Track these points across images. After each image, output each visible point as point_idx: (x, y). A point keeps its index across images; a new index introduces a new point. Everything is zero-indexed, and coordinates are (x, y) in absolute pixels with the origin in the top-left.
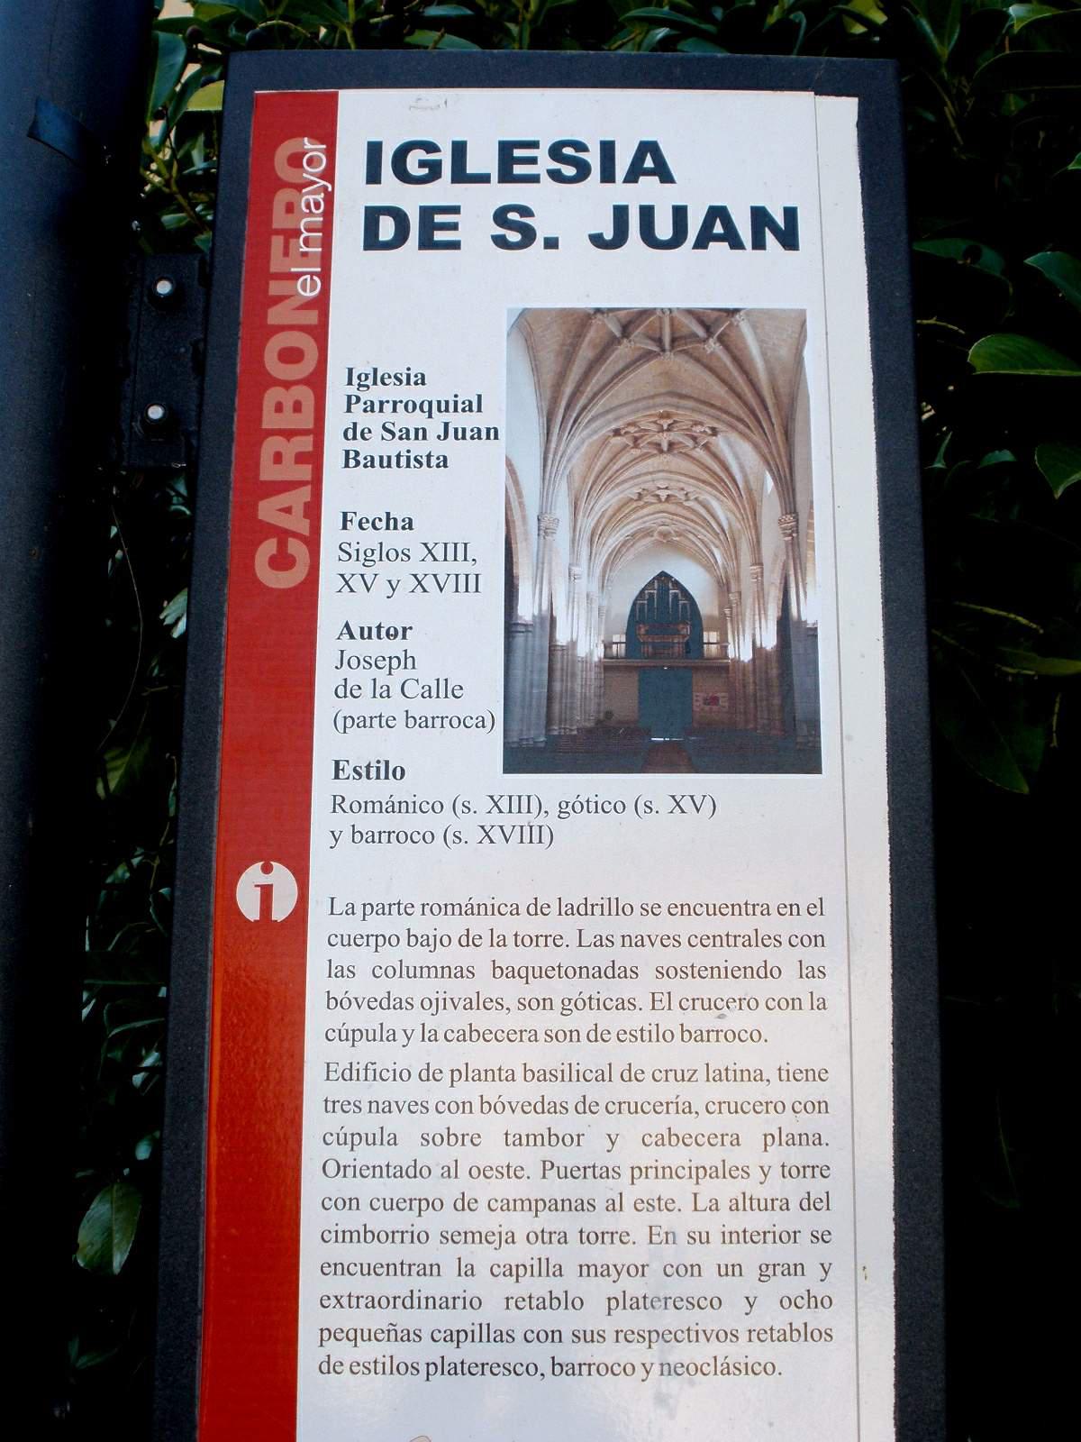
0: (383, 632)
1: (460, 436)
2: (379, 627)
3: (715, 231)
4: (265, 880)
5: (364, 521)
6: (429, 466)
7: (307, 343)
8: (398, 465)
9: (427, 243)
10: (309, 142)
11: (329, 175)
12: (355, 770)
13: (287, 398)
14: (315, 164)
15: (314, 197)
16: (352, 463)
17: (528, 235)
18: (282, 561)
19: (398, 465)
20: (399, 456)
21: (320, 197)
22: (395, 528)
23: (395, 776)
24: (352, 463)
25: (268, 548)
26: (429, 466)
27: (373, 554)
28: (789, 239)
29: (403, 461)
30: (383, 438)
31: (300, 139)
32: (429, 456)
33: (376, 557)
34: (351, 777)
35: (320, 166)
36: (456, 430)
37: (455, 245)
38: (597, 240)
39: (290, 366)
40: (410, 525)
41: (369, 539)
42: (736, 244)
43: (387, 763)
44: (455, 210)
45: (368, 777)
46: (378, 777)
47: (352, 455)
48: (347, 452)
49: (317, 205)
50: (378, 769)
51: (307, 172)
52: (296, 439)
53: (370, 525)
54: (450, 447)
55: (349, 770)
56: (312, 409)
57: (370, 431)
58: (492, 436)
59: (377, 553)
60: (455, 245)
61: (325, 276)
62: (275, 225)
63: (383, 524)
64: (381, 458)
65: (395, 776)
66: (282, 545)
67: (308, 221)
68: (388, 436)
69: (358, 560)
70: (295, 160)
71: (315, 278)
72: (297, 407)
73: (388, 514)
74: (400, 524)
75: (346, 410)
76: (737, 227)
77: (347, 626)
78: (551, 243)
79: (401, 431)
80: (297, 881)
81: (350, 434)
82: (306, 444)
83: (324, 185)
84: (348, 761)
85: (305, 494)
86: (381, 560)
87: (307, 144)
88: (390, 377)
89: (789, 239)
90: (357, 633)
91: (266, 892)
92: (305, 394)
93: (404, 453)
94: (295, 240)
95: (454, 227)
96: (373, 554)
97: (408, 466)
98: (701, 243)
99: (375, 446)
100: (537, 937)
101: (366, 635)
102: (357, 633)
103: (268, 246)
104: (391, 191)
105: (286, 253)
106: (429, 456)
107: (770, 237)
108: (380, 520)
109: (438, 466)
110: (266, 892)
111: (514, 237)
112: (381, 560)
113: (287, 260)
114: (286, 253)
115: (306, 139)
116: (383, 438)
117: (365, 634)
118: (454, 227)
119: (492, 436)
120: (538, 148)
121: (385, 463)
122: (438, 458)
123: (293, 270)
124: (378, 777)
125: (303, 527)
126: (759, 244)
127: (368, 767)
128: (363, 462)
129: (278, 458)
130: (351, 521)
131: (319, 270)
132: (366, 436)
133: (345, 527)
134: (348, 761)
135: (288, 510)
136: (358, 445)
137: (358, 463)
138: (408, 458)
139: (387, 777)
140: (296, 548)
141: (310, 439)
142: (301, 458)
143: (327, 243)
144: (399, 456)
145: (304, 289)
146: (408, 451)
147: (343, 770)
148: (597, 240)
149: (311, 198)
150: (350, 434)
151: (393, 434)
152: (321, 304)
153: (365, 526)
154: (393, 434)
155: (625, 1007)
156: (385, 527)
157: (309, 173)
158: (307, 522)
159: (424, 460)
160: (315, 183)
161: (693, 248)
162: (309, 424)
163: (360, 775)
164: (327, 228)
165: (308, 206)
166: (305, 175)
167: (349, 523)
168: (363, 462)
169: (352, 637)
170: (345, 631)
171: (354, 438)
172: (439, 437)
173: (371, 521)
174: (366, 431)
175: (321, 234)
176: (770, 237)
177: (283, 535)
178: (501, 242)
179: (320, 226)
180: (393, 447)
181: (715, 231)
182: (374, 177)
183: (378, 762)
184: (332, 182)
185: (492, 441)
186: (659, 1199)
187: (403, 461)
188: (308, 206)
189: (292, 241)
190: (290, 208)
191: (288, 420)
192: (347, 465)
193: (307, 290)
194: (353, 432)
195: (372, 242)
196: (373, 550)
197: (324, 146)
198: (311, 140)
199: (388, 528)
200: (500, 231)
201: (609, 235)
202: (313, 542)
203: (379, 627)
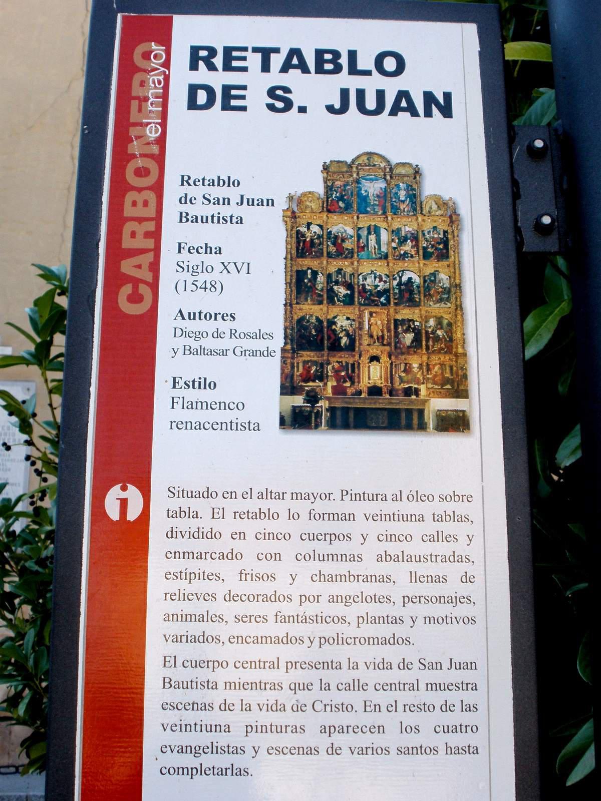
0: (203, 315)
1: (250, 203)
2: (200, 313)
3: (402, 105)
4: (123, 495)
5: (192, 248)
6: (231, 222)
7: (153, 166)
8: (213, 222)
9: (226, 107)
10: (155, 45)
11: (167, 64)
12: (185, 383)
13: (139, 198)
14: (158, 57)
15: (158, 77)
16: (184, 220)
17: (289, 105)
18: (136, 298)
19: (213, 222)
20: (213, 217)
21: (161, 78)
22: (211, 253)
23: (206, 319)
24: (184, 220)
25: (127, 289)
26: (231, 222)
27: (198, 268)
28: (446, 111)
29: (216, 219)
30: (203, 203)
31: (150, 43)
32: (231, 217)
33: (200, 270)
34: (183, 388)
35: (161, 59)
36: (248, 200)
37: (244, 109)
38: (330, 109)
39: (143, 179)
40: (220, 251)
41: (195, 259)
42: (415, 113)
43: (205, 379)
44: (244, 88)
45: (194, 388)
46: (200, 388)
47: (184, 215)
48: (181, 213)
49: (159, 83)
50: (200, 383)
51: (154, 63)
52: (145, 223)
53: (195, 251)
54: (244, 211)
55: (182, 383)
56: (155, 205)
57: (195, 199)
58: (270, 204)
59: (200, 268)
60: (244, 109)
61: (164, 124)
62: (134, 94)
63: (203, 251)
64: (202, 217)
65: (206, 319)
66: (135, 288)
67: (152, 92)
68: (206, 202)
69: (188, 271)
70: (146, 56)
71: (157, 126)
72: (146, 204)
73: (206, 244)
74: (214, 251)
75: (179, 221)
76: (418, 109)
77: (180, 311)
78: (302, 110)
79: (214, 199)
80: (144, 499)
81: (183, 201)
82: (151, 226)
83: (164, 71)
84: (181, 378)
85: (150, 257)
86: (202, 272)
87: (154, 46)
88: (227, 315)
89: (446, 111)
90: (186, 316)
91: (124, 503)
92: (151, 196)
93: (216, 214)
94: (145, 103)
95: (243, 97)
96: (198, 268)
97: (219, 222)
98: (394, 112)
99: (198, 209)
100: (323, 514)
101: (192, 317)
102: (186, 316)
103: (129, 107)
104: (203, 75)
105: (140, 110)
106: (231, 217)
107: (435, 110)
108: (202, 248)
109: (237, 223)
110: (124, 503)
111: (280, 105)
112: (202, 272)
113: (141, 115)
114: (140, 110)
115: (153, 43)
116: (203, 203)
117: (192, 317)
118: (243, 97)
119: (270, 204)
120: (279, 53)
121: (205, 220)
122: (237, 218)
123: (144, 121)
124: (200, 388)
125: (149, 277)
126: (428, 114)
127: (194, 381)
128: (191, 219)
129: (133, 235)
130: (184, 248)
131: (160, 121)
132: (193, 202)
133: (180, 252)
134: (181, 378)
135: (139, 267)
136: (187, 208)
137: (187, 220)
138: (219, 218)
139: (205, 388)
140: (144, 290)
141: (153, 223)
142: (147, 235)
143: (165, 105)
144: (213, 217)
145: (151, 132)
146: (219, 213)
147: (178, 383)
148: (330, 109)
149: (156, 78)
150: (183, 201)
151: (210, 201)
152: (161, 141)
153: (192, 251)
154: (210, 201)
155: (460, 752)
156: (204, 252)
157: (155, 63)
158: (151, 274)
159: (228, 219)
160: (159, 69)
161: (389, 115)
162: (151, 212)
163: (189, 386)
164: (165, 97)
165: (154, 83)
166: (152, 64)
167: (182, 249)
168: (191, 219)
169: (183, 318)
170: (179, 315)
171: (186, 203)
172: (238, 204)
173: (196, 249)
174: (193, 199)
175: (161, 100)
176: (435, 110)
177: (136, 282)
178: (271, 107)
179: (161, 95)
180: (210, 210)
181: (402, 105)
182: (194, 67)
183: (200, 378)
184: (169, 69)
185: (270, 207)
186: (424, 704)
187: (216, 219)
188: (154, 83)
189: (143, 104)
190: (142, 84)
191: (140, 212)
192: (181, 221)
193: (152, 133)
194: (185, 200)
195: (192, 104)
196: (197, 266)
197: (164, 48)
198: (157, 44)
199: (206, 253)
200: (271, 101)
201: (337, 106)
202: (154, 286)
203: (200, 313)
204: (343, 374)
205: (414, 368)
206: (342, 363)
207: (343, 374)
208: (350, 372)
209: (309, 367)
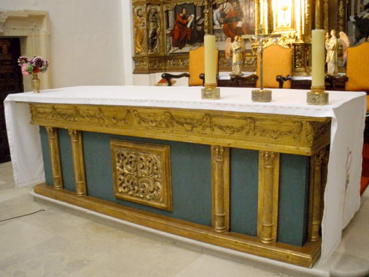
209: (185, 18)
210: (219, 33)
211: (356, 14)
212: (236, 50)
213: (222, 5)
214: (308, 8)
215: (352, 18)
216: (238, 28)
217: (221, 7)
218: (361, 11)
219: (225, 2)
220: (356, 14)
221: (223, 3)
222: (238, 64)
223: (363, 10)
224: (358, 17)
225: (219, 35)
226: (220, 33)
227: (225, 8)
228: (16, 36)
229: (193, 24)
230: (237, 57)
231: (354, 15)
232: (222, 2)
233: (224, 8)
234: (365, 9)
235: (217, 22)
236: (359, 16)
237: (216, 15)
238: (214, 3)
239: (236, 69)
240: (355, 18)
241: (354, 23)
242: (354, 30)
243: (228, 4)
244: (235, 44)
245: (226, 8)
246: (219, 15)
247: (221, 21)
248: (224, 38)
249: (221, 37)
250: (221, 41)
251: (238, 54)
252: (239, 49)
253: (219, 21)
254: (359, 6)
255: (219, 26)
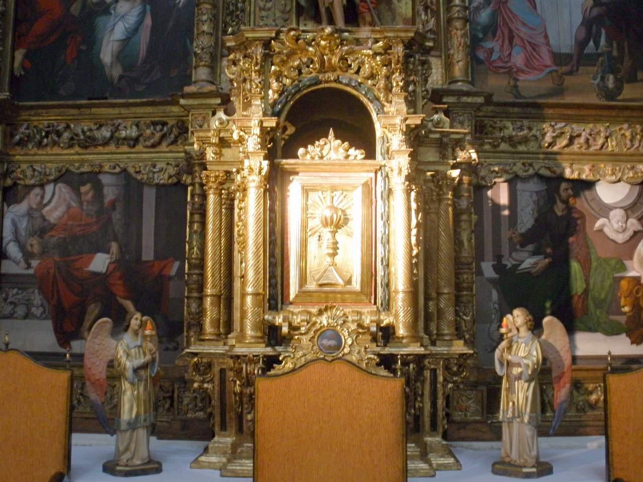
204: (100, 263)
205: (605, 210)
206: (98, 188)
207: (100, 263)
208: (148, 254)
210: (19, 289)
211: (498, 257)
212: (136, 370)
213: (37, 190)
214: (418, 225)
215: (488, 269)
216: (96, 274)
217: (33, 198)
218: (513, 249)
219: (49, 182)
220: (498, 257)
221: (42, 186)
222: (143, 427)
223: (518, 247)
224: (506, 265)
225: (19, 297)
226: (24, 289)
227: (50, 202)
228: (287, 224)
229: (468, 355)
230: (138, 398)
231: (494, 260)
232: (41, 180)
233: (45, 201)
234: (523, 245)
235: (13, 249)
236: (509, 263)
237: (14, 224)
238: (9, 182)
239: (133, 446)
240: (495, 268)
241: (491, 281)
242: (495, 303)
243: (60, 188)
244: (132, 345)
245: (52, 204)
246: (23, 224)
247: (29, 248)
248: (37, 307)
249: (28, 304)
250: (26, 317)
251: (141, 389)
252: (144, 367)
253: (22, 247)
254: (505, 234)
255: (23, 264)
